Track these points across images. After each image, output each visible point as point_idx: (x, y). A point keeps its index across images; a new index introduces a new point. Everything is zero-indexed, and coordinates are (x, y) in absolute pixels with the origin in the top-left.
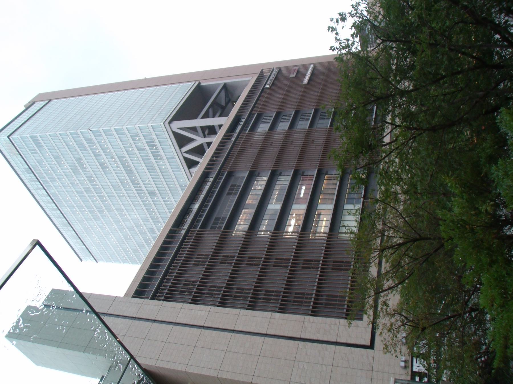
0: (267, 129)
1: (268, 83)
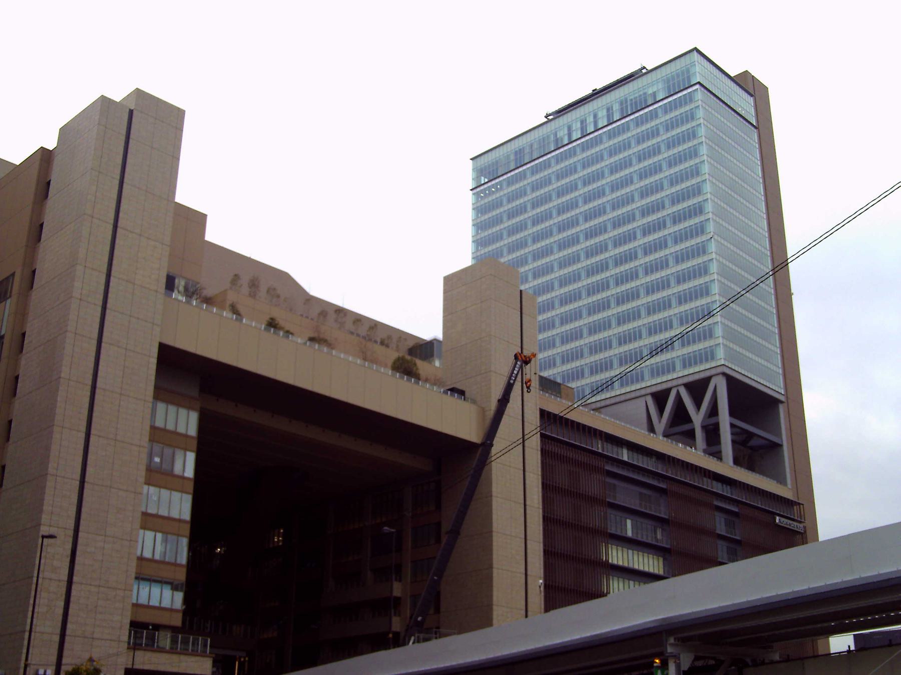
0: (718, 532)
1: (783, 519)
